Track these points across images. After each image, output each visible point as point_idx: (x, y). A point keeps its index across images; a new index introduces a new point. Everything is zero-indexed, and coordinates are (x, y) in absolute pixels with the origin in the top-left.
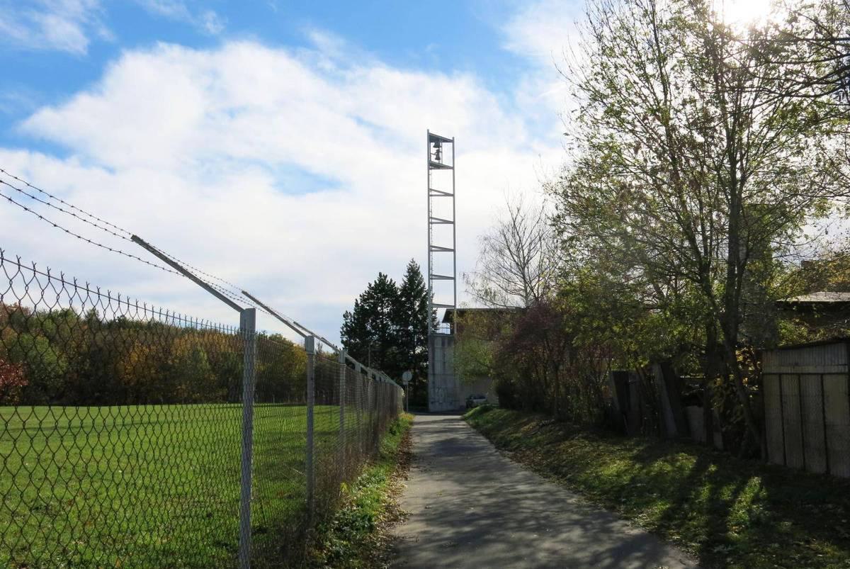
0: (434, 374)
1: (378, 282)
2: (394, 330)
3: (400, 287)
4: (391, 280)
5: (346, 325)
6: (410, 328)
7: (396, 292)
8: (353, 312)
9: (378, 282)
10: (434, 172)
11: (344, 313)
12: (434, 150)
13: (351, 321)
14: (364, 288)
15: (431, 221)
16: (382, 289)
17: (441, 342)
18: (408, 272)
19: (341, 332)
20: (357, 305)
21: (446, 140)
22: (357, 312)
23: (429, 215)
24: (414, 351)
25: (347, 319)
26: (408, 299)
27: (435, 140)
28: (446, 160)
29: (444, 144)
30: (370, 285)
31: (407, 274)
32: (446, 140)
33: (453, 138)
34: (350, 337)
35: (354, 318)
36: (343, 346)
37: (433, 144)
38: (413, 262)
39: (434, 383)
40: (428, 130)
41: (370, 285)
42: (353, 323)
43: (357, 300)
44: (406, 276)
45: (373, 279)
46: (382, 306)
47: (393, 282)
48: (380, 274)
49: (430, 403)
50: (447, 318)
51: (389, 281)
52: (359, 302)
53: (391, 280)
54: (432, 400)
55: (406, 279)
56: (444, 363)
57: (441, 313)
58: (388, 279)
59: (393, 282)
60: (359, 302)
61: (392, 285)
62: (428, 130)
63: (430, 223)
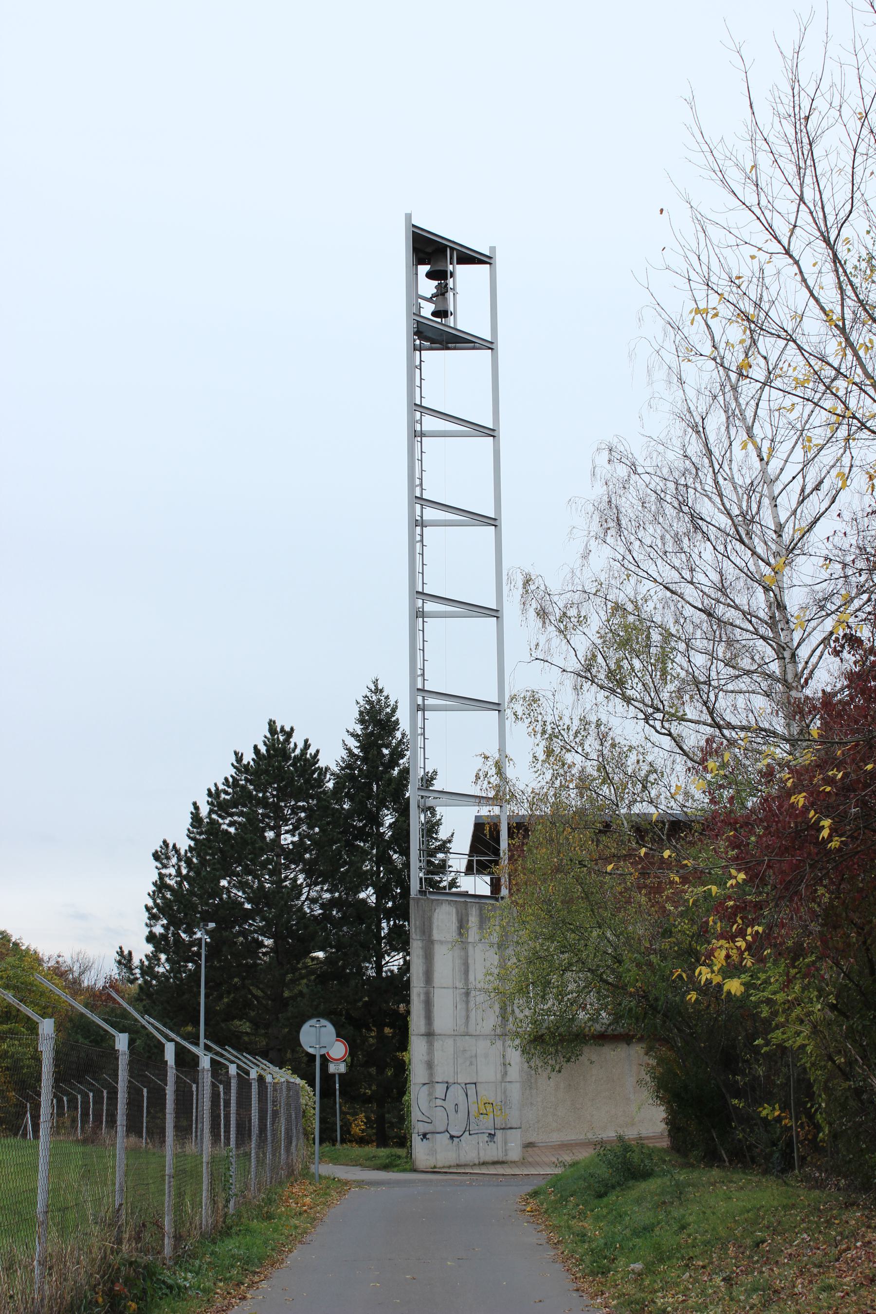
0: (430, 1035)
1: (263, 749)
2: (314, 901)
3: (336, 769)
4: (307, 745)
5: (161, 886)
6: (368, 895)
7: (320, 782)
8: (185, 845)
9: (263, 749)
10: (434, 359)
11: (157, 846)
12: (428, 287)
13: (179, 872)
14: (221, 771)
15: (421, 604)
16: (278, 767)
17: (454, 925)
18: (362, 721)
19: (148, 908)
20: (196, 818)
21: (469, 258)
22: (198, 848)
23: (414, 480)
24: (379, 968)
25: (165, 866)
26: (360, 809)
27: (431, 252)
28: (467, 317)
29: (463, 272)
30: (239, 758)
31: (358, 729)
32: (469, 258)
33: (493, 249)
34: (174, 922)
35: (189, 862)
36: (149, 948)
37: (424, 269)
38: (378, 691)
39: (430, 1065)
40: (408, 217)
41: (239, 758)
42: (186, 878)
43: (196, 808)
44: (354, 735)
45: (251, 740)
46: (276, 828)
47: (312, 751)
48: (272, 724)
49: (414, 1136)
50: (484, 839)
51: (301, 745)
52: (204, 810)
53: (307, 745)
54: (421, 1128)
55: (353, 743)
56: (467, 994)
57: (457, 826)
58: (297, 740)
59: (312, 751)
60: (204, 810)
61: (307, 763)
62: (408, 217)
63: (417, 435)
